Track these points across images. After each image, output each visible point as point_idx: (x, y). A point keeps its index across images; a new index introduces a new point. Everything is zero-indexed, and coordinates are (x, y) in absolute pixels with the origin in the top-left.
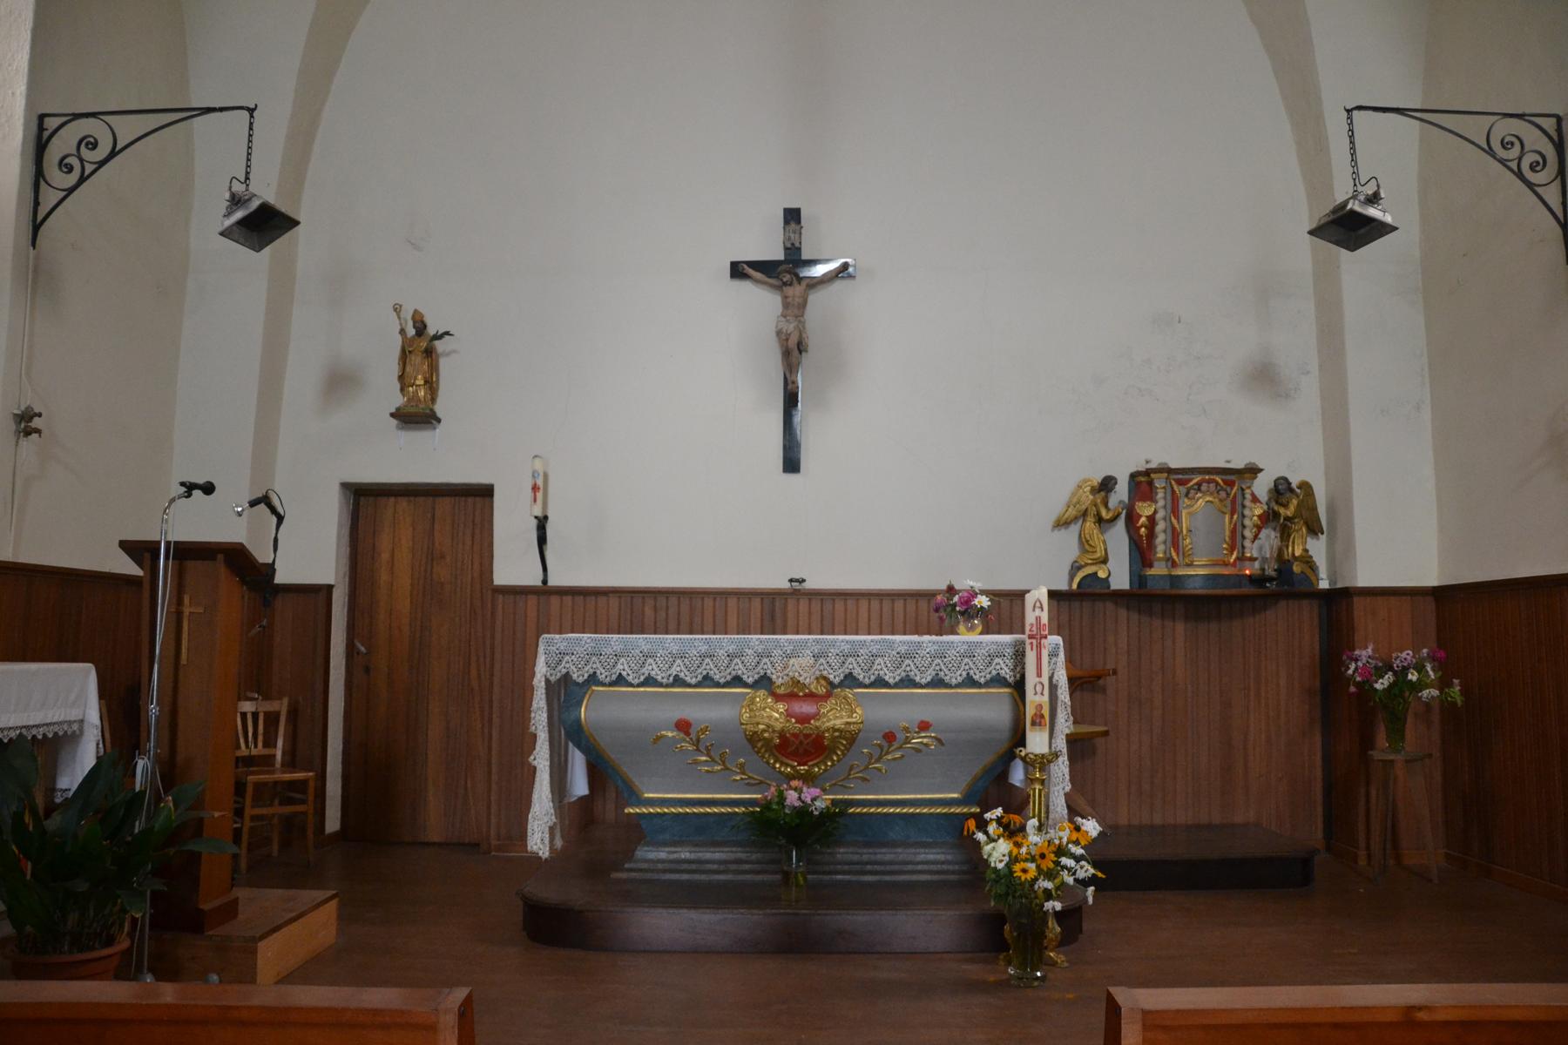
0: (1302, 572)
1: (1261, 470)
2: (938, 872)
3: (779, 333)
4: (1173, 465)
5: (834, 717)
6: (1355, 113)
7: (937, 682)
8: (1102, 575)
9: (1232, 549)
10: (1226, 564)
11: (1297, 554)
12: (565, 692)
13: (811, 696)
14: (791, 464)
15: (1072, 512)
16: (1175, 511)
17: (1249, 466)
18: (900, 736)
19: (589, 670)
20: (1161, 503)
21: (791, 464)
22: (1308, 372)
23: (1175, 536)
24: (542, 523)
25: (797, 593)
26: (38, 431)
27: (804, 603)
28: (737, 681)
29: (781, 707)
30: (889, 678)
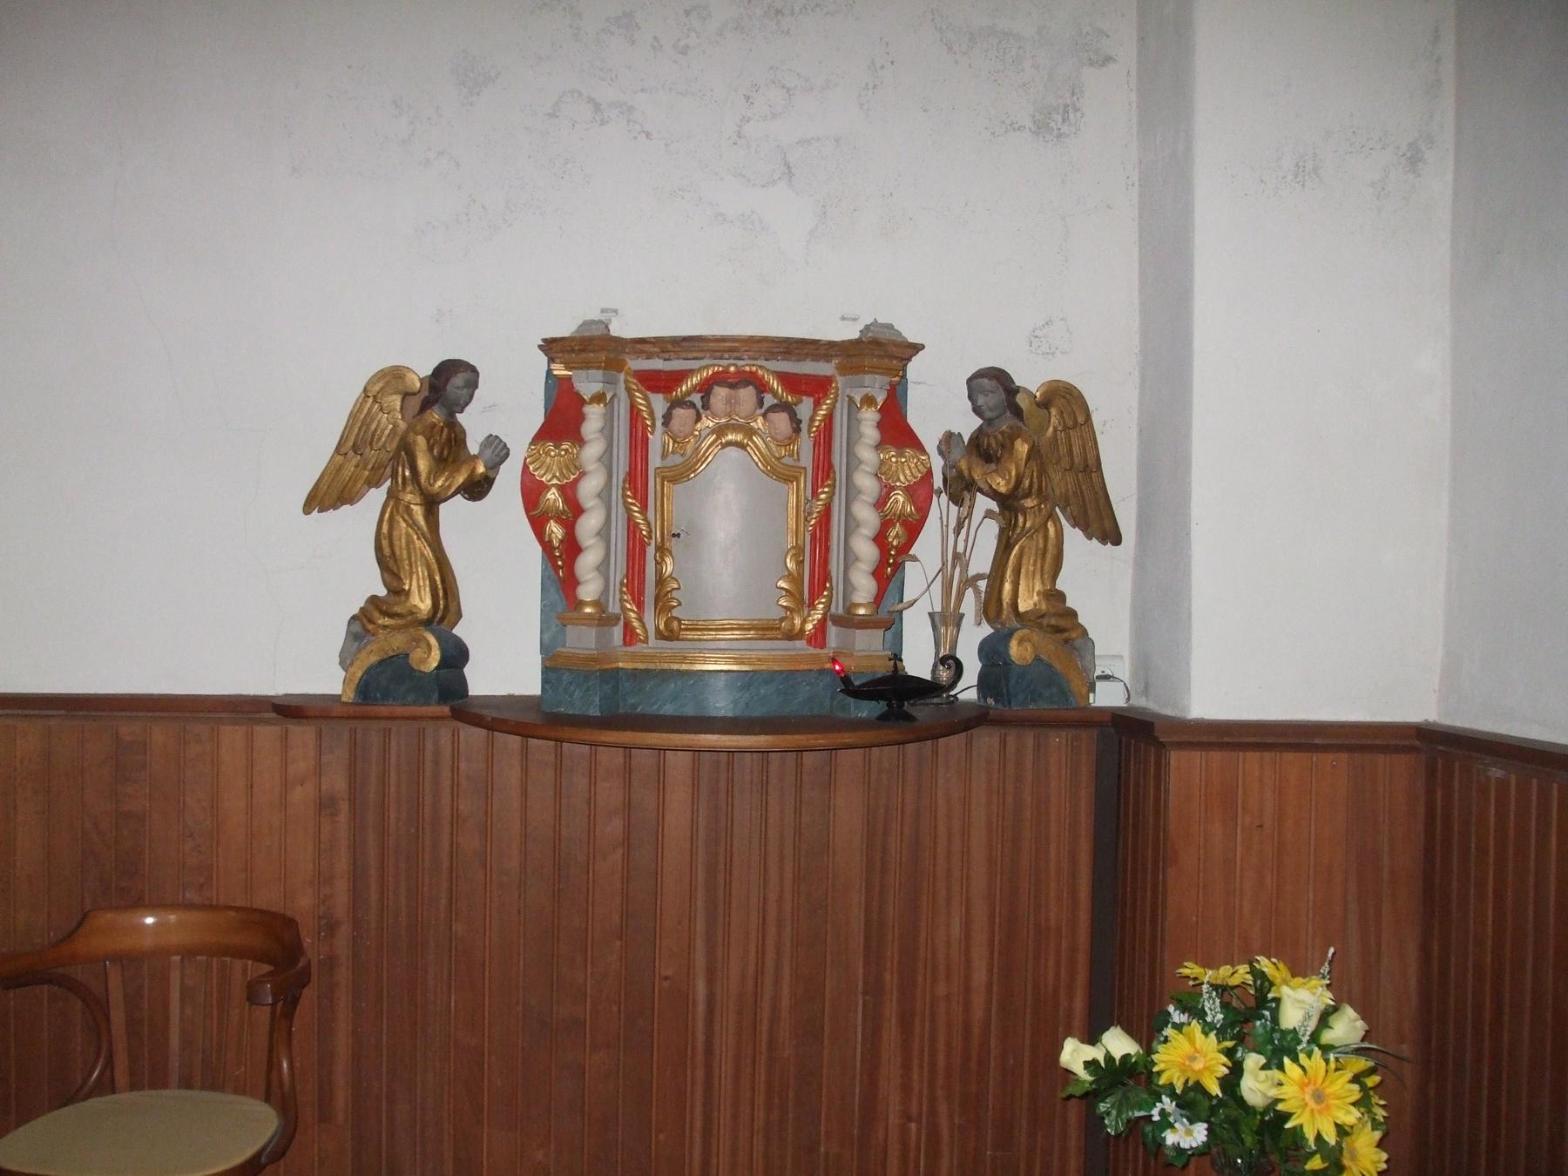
0: (1038, 659)
1: (917, 348)
11: (1023, 606)
17: (884, 336)
20: (592, 451)
22: (1108, 59)
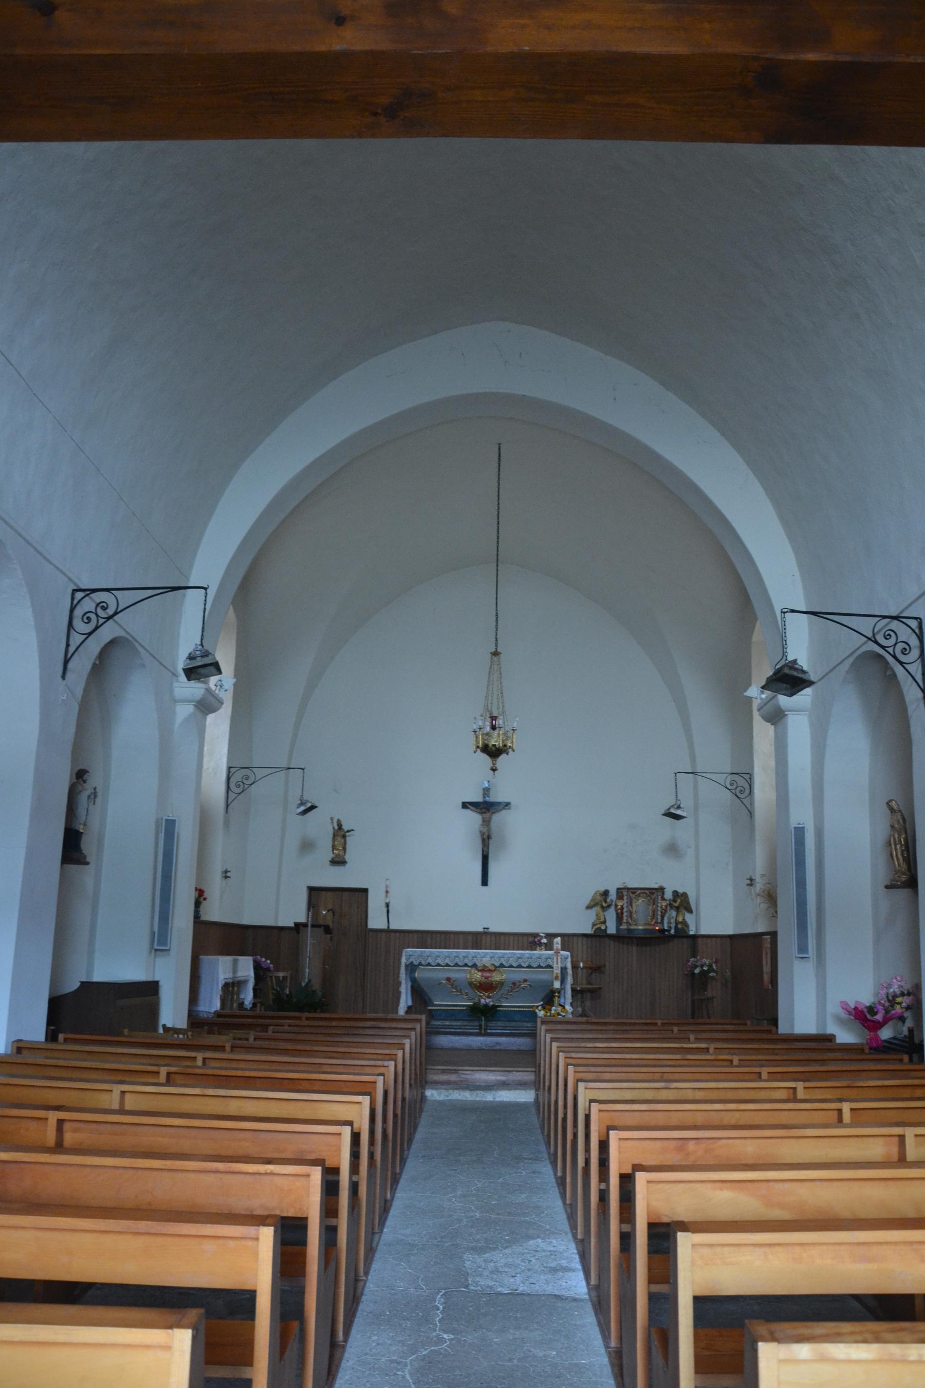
2: (529, 1030)
3: (481, 832)
4: (629, 887)
5: (496, 977)
6: (678, 774)
7: (529, 967)
8: (603, 928)
9: (652, 920)
10: (650, 925)
12: (411, 968)
13: (490, 971)
14: (485, 882)
15: (592, 903)
16: (630, 903)
18: (518, 984)
19: (419, 961)
21: (485, 882)
23: (630, 914)
24: (387, 905)
25: (486, 933)
26: (229, 877)
27: (488, 938)
28: (466, 965)
29: (480, 973)
30: (514, 965)
